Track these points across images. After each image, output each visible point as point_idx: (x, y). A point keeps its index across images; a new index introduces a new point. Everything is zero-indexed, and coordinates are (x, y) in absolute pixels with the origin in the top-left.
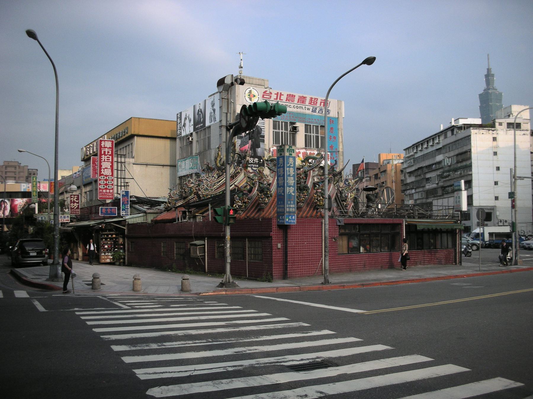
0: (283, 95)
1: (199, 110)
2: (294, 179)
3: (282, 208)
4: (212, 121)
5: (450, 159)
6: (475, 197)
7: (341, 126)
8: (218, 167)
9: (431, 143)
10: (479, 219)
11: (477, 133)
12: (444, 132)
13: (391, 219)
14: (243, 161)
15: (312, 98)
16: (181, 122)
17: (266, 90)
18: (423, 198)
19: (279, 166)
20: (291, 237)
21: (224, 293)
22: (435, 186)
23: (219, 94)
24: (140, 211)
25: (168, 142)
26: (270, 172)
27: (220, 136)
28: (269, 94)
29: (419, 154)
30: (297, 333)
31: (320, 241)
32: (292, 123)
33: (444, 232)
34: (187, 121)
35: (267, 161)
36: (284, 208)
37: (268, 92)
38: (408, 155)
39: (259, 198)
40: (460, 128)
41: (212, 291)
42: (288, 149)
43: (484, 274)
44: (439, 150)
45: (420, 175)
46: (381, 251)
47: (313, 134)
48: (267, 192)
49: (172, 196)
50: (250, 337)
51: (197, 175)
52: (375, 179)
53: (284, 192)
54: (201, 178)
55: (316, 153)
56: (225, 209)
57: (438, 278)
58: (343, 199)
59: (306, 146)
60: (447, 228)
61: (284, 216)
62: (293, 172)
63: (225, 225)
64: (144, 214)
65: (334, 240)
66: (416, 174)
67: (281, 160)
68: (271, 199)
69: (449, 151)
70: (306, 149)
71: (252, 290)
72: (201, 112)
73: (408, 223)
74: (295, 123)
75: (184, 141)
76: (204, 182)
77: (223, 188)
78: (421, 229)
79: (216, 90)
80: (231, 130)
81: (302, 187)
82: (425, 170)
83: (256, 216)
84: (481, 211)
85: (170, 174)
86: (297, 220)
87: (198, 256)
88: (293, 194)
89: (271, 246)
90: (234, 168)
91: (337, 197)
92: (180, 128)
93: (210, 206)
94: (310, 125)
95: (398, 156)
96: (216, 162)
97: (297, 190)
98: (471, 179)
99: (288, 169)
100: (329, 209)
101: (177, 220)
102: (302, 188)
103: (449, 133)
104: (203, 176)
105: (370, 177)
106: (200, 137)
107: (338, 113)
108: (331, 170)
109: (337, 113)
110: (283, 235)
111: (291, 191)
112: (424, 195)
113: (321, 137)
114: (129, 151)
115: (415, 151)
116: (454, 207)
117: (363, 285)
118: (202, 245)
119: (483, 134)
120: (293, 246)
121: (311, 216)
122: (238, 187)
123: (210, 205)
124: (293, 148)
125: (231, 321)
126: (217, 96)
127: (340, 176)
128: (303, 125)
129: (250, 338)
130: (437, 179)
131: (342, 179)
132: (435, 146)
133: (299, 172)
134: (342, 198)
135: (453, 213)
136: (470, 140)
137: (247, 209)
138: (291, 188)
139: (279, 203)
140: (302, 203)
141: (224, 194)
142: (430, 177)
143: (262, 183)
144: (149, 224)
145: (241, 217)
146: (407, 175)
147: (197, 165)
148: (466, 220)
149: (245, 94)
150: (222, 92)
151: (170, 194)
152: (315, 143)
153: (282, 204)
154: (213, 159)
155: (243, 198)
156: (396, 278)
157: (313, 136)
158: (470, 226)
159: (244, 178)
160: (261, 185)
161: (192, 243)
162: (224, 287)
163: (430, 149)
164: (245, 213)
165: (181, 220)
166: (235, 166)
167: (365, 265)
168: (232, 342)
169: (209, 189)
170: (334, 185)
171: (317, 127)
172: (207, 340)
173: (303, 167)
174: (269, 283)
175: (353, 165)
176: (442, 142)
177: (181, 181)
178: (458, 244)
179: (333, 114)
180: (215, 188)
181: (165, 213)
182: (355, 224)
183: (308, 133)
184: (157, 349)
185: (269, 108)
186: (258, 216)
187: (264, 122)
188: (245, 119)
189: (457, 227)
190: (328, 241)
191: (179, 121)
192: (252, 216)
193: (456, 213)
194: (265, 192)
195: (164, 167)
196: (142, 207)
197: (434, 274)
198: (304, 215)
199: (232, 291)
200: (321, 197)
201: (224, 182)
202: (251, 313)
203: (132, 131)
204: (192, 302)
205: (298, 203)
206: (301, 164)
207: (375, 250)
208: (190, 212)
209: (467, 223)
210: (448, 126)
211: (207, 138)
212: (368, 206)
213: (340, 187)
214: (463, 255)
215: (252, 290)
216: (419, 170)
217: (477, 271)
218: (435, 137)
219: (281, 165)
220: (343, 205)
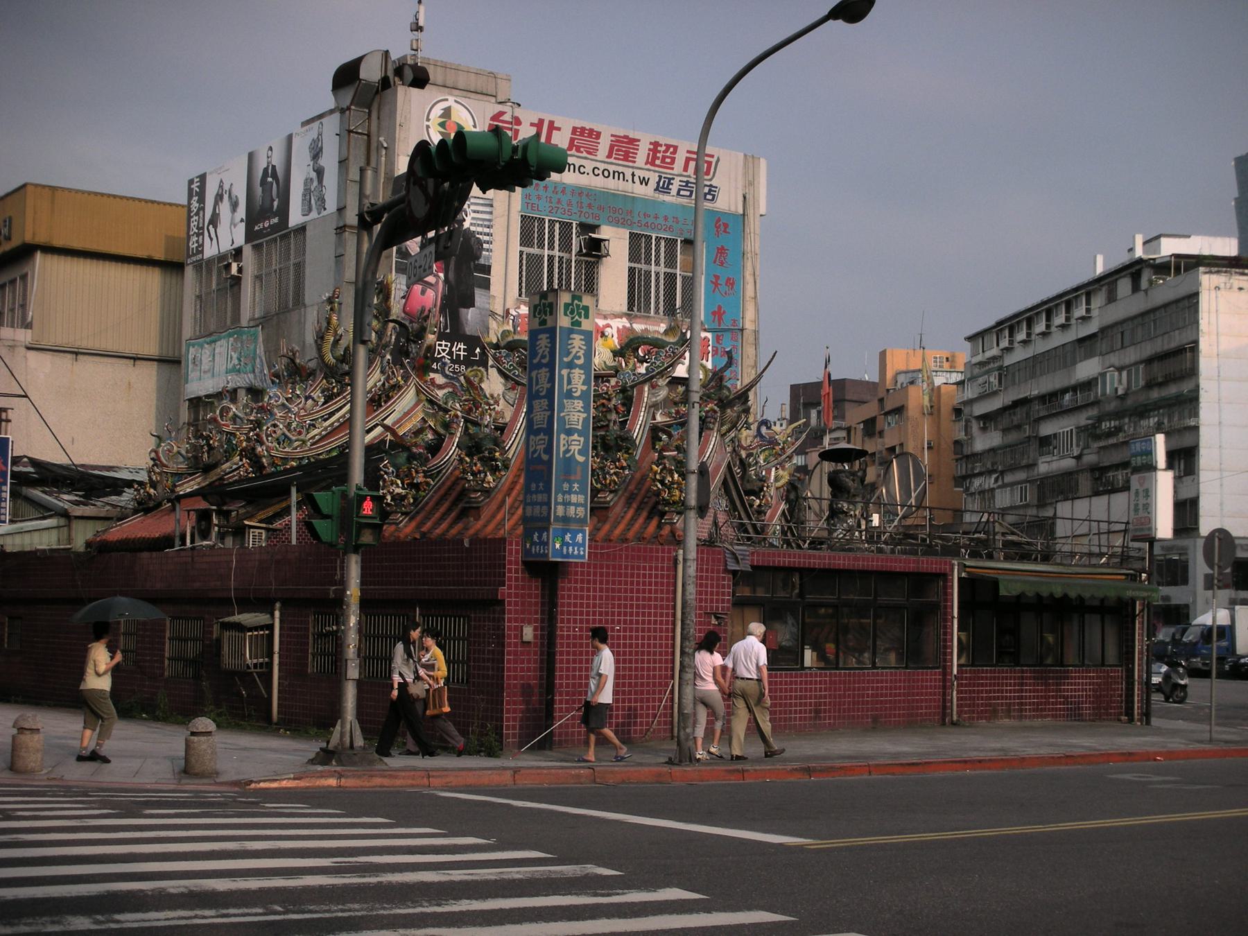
0: (559, 129)
1: (266, 170)
2: (586, 408)
3: (541, 504)
4: (310, 210)
5: (1124, 374)
6: (1205, 505)
7: (754, 242)
8: (327, 365)
9: (1060, 319)
10: (1211, 566)
11: (1222, 286)
12: (1107, 281)
13: (912, 558)
14: (413, 348)
15: (656, 144)
16: (203, 209)
17: (500, 108)
18: (1026, 506)
19: (535, 361)
20: (569, 605)
21: (332, 782)
22: (1069, 463)
23: (337, 115)
24: (45, 511)
25: (153, 279)
26: (505, 385)
27: (337, 262)
28: (511, 123)
29: (1019, 355)
30: (576, 894)
31: (667, 623)
32: (586, 228)
33: (1092, 610)
34: (225, 208)
35: (497, 346)
36: (548, 504)
37: (507, 117)
38: (979, 358)
39: (465, 471)
40: (1162, 268)
41: (292, 776)
42: (567, 306)
43: (1225, 754)
44: (1088, 343)
45: (1018, 427)
46: (874, 663)
47: (657, 269)
48: (492, 451)
49: (165, 462)
50: (417, 902)
51: (256, 393)
52: (864, 436)
53: (549, 450)
54: (266, 399)
55: (663, 327)
56: (344, 495)
57: (1069, 759)
58: (749, 487)
59: (630, 308)
60: (1100, 594)
61: (548, 532)
62: (583, 384)
63: (345, 553)
64: (62, 521)
65: (714, 621)
66: (1005, 421)
67: (543, 340)
68: (507, 477)
69: (1122, 347)
70: (629, 316)
71: (429, 777)
72: (274, 175)
73: (968, 572)
74: (598, 226)
75: (211, 277)
76: (279, 414)
77: (340, 439)
78: (1014, 593)
79: (329, 102)
80: (378, 228)
81: (611, 438)
82: (1038, 409)
83: (453, 531)
84: (1220, 539)
85: (159, 389)
86: (590, 547)
87: (248, 667)
88: (580, 459)
89: (500, 632)
90: (382, 372)
91: (729, 480)
92: (198, 228)
93: (294, 496)
94: (649, 238)
95: (947, 359)
96: (319, 349)
97: (594, 448)
98: (1193, 445)
99: (565, 372)
100: (702, 510)
101: (177, 542)
102: (612, 443)
103: (1124, 286)
104: (275, 396)
105: (849, 430)
106: (269, 264)
107: (745, 197)
108: (713, 384)
109: (741, 199)
110: (543, 597)
111: (575, 448)
112: (1031, 496)
113: (684, 278)
114: (14, 303)
115: (1005, 343)
116: (1131, 526)
117: (809, 771)
118: (262, 628)
119: (1241, 289)
120: (575, 637)
121: (640, 538)
122: (394, 433)
123: (294, 490)
124: (587, 300)
125: (351, 855)
126: (332, 125)
127: (743, 407)
128: (625, 234)
129: (416, 903)
130: (1078, 440)
131: (751, 420)
132: (1074, 328)
133: (603, 388)
134: (748, 481)
135: (1123, 547)
136: (1197, 311)
137: (422, 508)
138: (576, 437)
139: (534, 486)
140: (611, 492)
141: (344, 454)
142: (1055, 435)
143: (476, 424)
144: (78, 554)
145: (402, 536)
146: (975, 427)
147: (254, 359)
148: (1173, 583)
149: (428, 120)
150: (349, 108)
151: (156, 452)
152: (662, 292)
153: (541, 492)
154: (310, 338)
155: (409, 470)
156: (920, 754)
157: (657, 274)
158: (1187, 606)
159: (416, 405)
160: (472, 430)
161: (227, 619)
162: (334, 763)
163: (1058, 339)
164: (413, 524)
165: (192, 541)
166: (385, 362)
167: (817, 712)
168: (352, 914)
169: (294, 438)
170: (723, 435)
171: (671, 243)
172: (267, 909)
173: (617, 371)
174: (487, 758)
175: (792, 387)
176: (1100, 314)
177: (197, 414)
178: (1141, 652)
179: (727, 201)
180: (313, 437)
181: (137, 519)
182: (789, 570)
183: (639, 262)
184: (90, 931)
185: (507, 154)
186: (459, 533)
187: (490, 220)
188: (424, 189)
189: (1136, 594)
190: (692, 618)
191: (195, 205)
192: (437, 531)
193: (1136, 545)
194: (486, 454)
195: (138, 362)
196: (56, 498)
197: (1050, 745)
198: (617, 532)
199: (359, 777)
200: (676, 476)
201: (348, 416)
202: (422, 836)
203: (30, 232)
204: (219, 805)
205: (595, 492)
206: (611, 363)
207: (853, 662)
208: (225, 514)
209: (1176, 595)
210: (1123, 259)
211: (292, 267)
212: (835, 513)
213: (740, 446)
214: (1157, 698)
215: (429, 777)
216: (1018, 410)
217: (1201, 742)
218: (1076, 297)
219: (543, 357)
220: (751, 506)
